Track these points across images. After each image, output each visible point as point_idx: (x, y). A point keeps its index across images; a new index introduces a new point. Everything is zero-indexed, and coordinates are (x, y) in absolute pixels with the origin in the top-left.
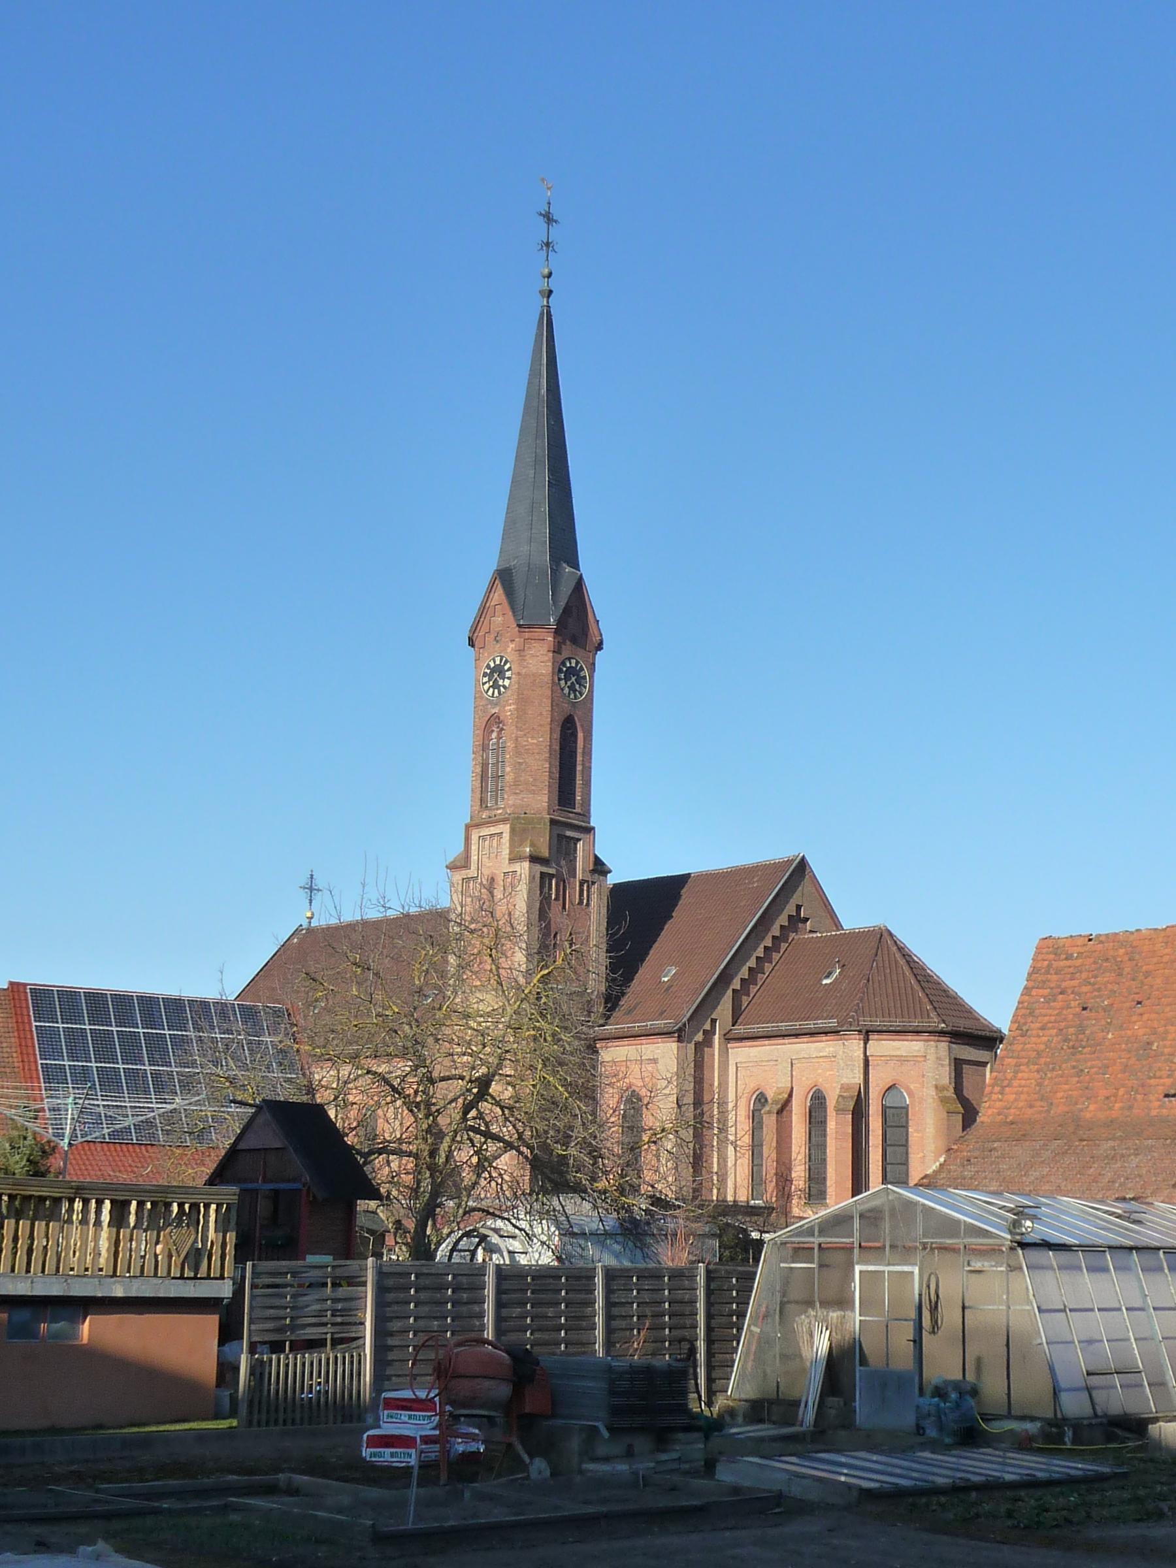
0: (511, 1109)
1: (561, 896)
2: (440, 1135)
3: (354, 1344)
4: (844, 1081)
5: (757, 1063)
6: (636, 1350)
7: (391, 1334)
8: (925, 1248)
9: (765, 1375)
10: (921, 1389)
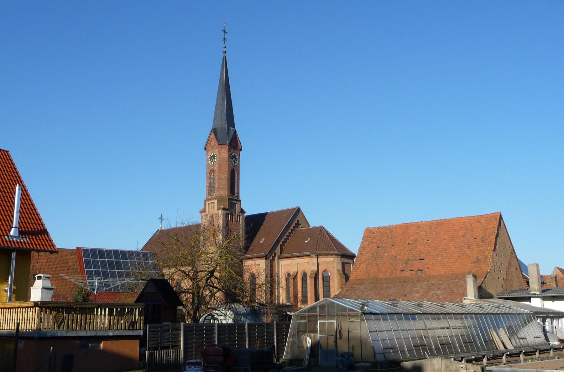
0: (220, 279)
1: (232, 219)
2: (200, 288)
5: (288, 265)
7: (188, 344)
10: (337, 354)
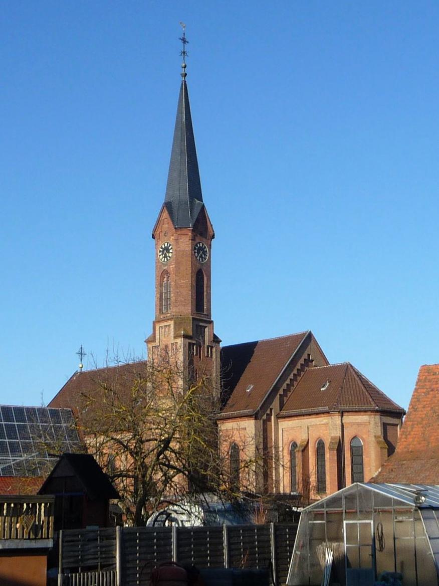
2: (146, 468)
3: (111, 567)
4: (333, 435)
5: (292, 428)
6: (243, 563)
7: (128, 562)
8: (375, 512)
9: (303, 573)
10: (376, 577)
